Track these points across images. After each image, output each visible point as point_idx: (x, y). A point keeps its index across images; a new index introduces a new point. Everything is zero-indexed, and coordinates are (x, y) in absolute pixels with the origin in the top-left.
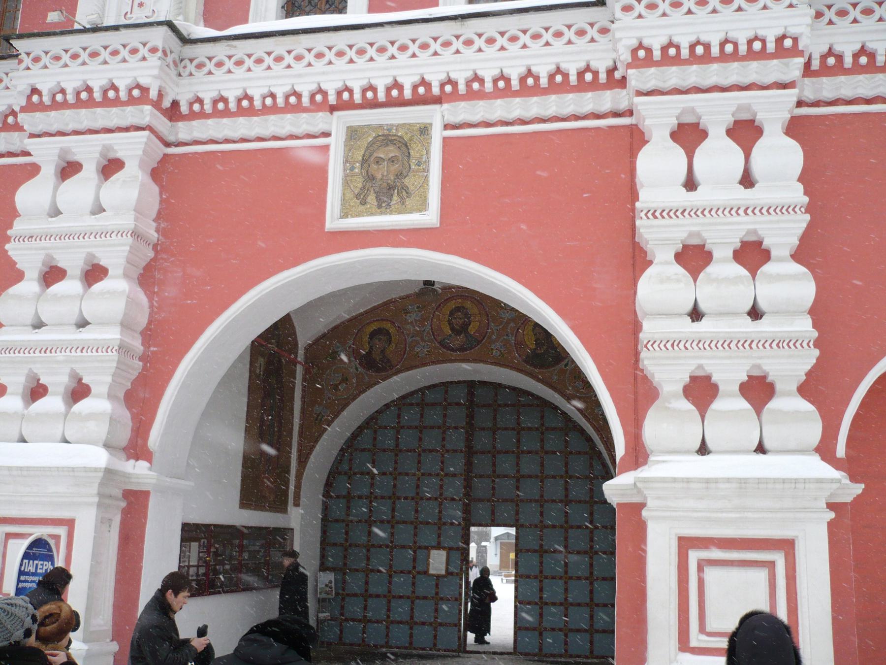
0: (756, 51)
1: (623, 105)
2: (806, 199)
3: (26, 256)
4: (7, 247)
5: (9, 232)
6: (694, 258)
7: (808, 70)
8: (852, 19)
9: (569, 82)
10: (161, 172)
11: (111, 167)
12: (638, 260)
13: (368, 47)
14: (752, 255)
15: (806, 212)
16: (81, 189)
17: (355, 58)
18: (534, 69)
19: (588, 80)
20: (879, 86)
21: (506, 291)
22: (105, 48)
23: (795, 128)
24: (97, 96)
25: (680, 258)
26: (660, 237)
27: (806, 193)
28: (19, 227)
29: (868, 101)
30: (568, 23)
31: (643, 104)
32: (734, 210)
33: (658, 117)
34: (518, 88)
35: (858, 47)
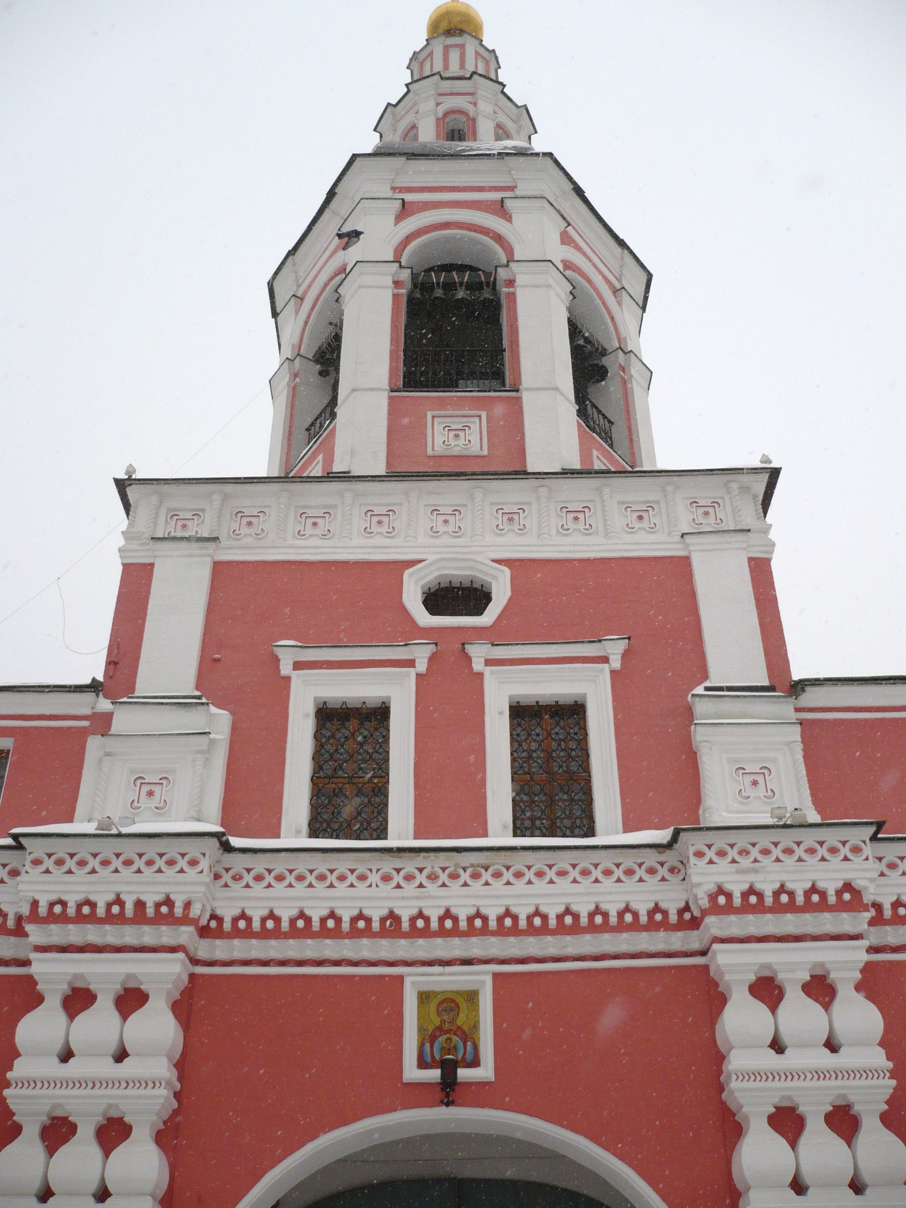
0: (816, 900)
1: (21, 955)
2: (890, 1065)
3: (28, 1105)
4: (6, 1092)
5: (9, 1075)
6: (58, 1132)
7: (878, 920)
8: (593, 879)
9: (371, 928)
10: (184, 1008)
11: (131, 1000)
12: (732, 1129)
13: (349, 873)
14: (844, 1121)
15: (891, 1077)
16: (100, 1024)
17: (402, 883)
18: (454, 911)
19: (657, 921)
20: (565, 947)
21: (371, 1132)
22: (50, 855)
23: (872, 982)
24: (71, 911)
25: (72, 1129)
26: (752, 1100)
27: (888, 1059)
28: (20, 1069)
29: (596, 958)
30: (843, 839)
31: (723, 951)
32: (819, 1074)
33: (736, 965)
34: (287, 929)
35: (652, 905)
